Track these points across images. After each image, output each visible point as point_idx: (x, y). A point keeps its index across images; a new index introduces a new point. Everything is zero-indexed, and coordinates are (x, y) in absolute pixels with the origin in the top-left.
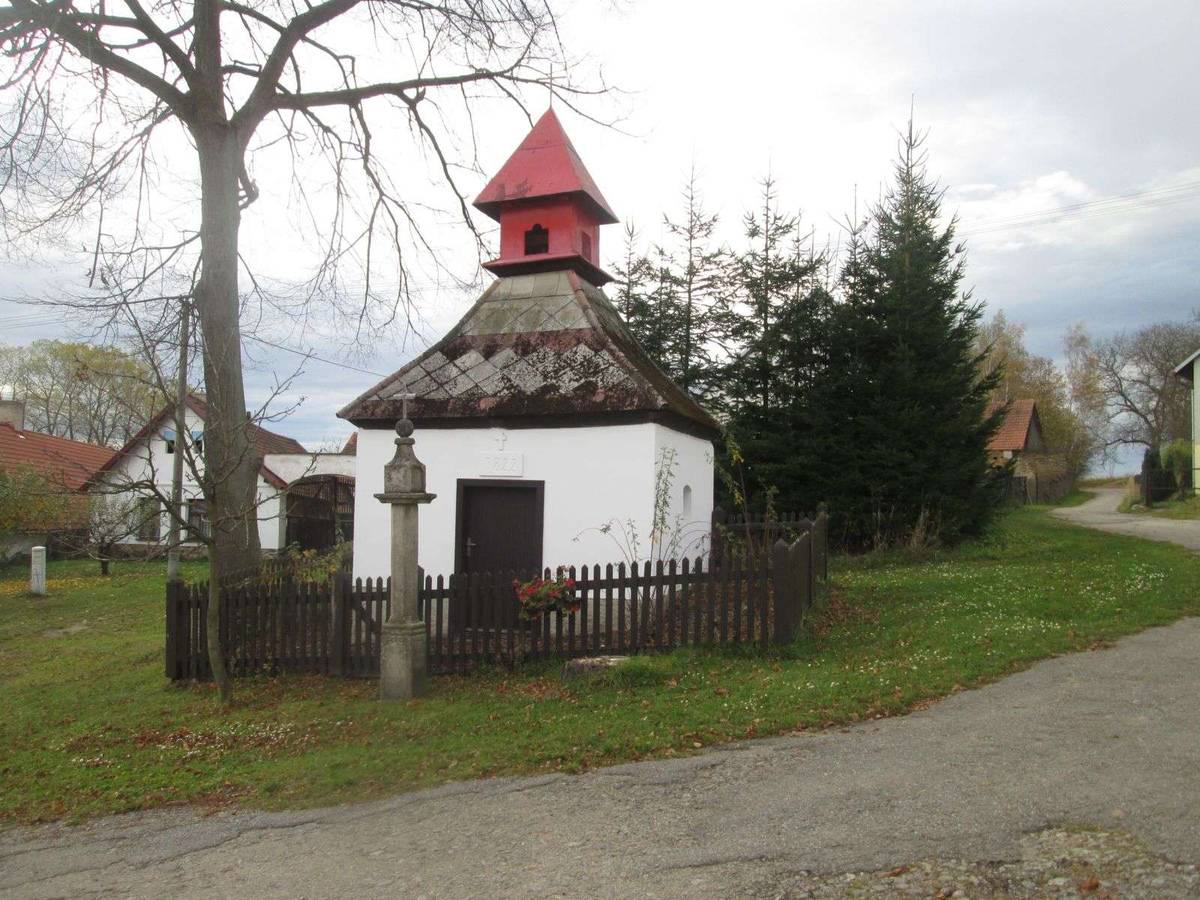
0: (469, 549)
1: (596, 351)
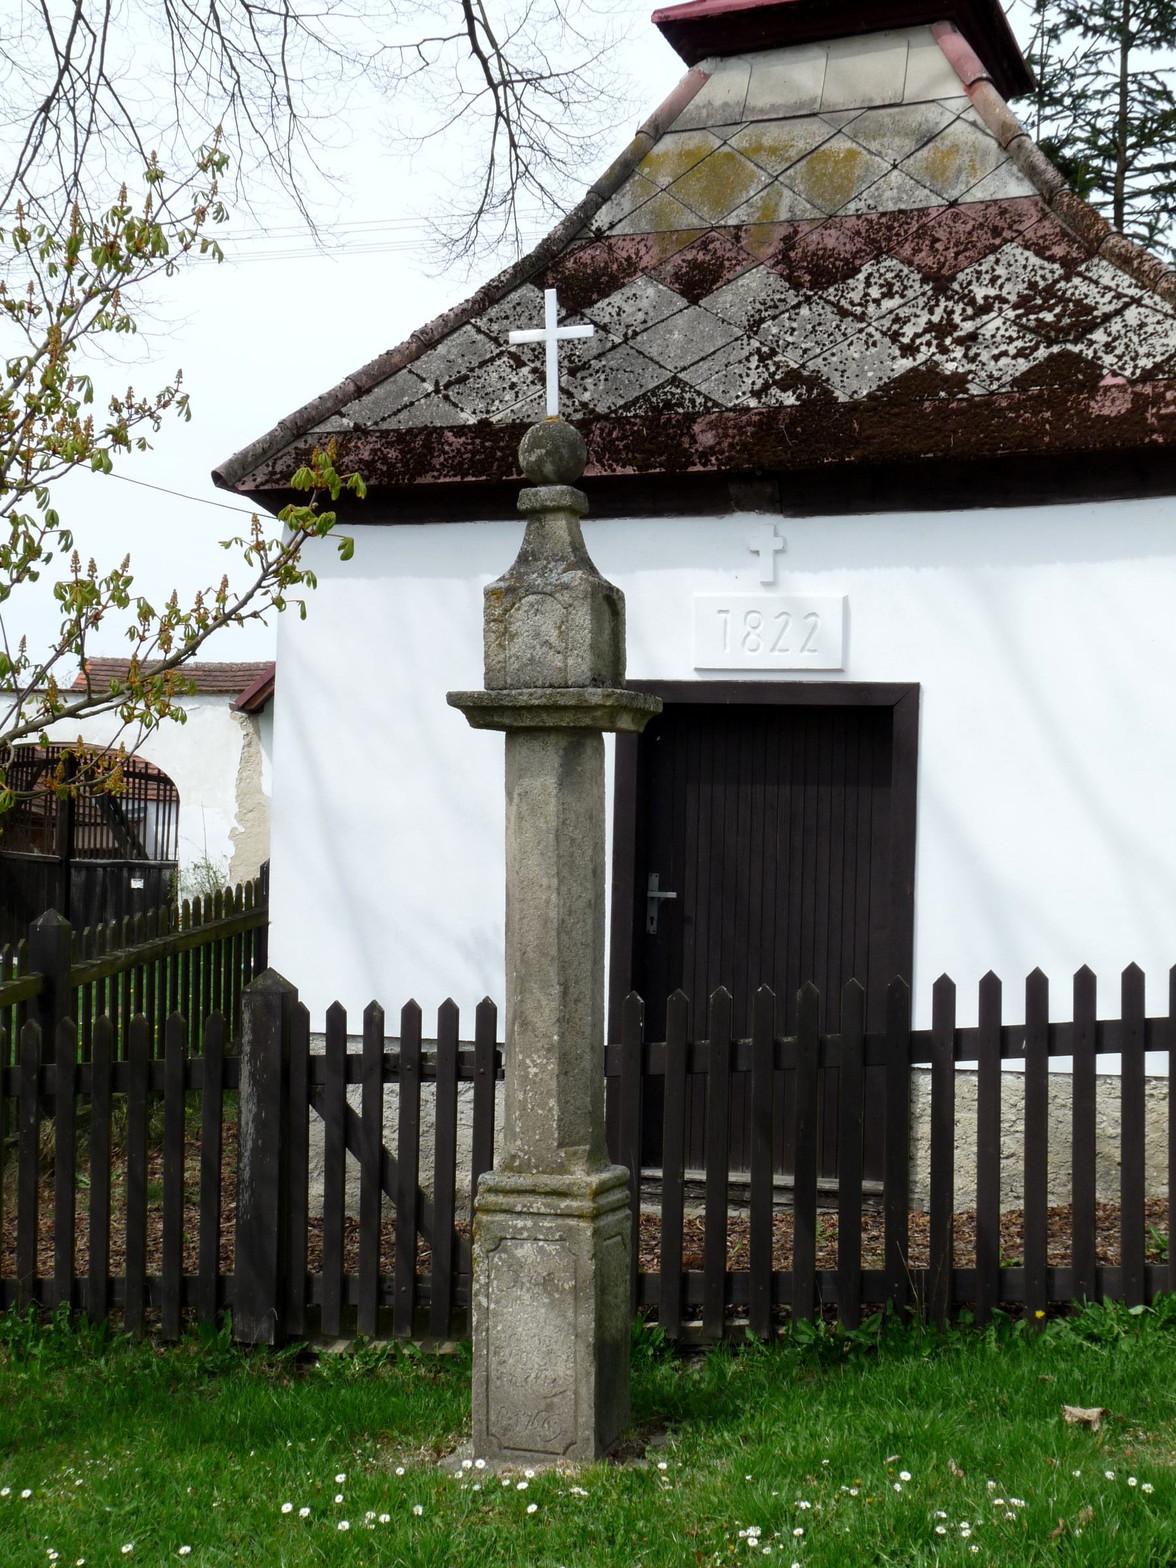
0: (653, 911)
1: (1070, 268)
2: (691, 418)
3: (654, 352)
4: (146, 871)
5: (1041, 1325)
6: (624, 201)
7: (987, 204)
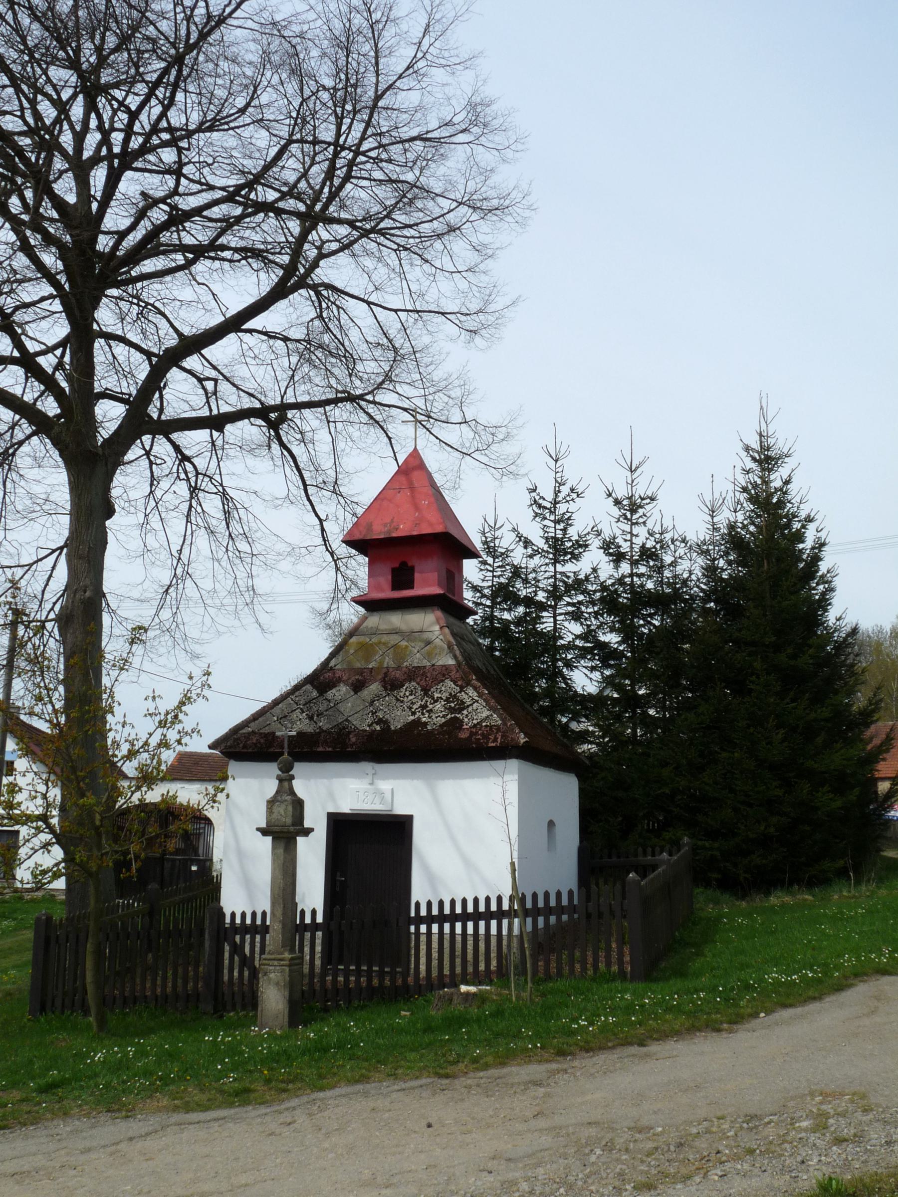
1: (462, 689)
2: (350, 733)
3: (342, 710)
4: (198, 862)
5: (417, 999)
6: (340, 657)
7: (443, 666)
